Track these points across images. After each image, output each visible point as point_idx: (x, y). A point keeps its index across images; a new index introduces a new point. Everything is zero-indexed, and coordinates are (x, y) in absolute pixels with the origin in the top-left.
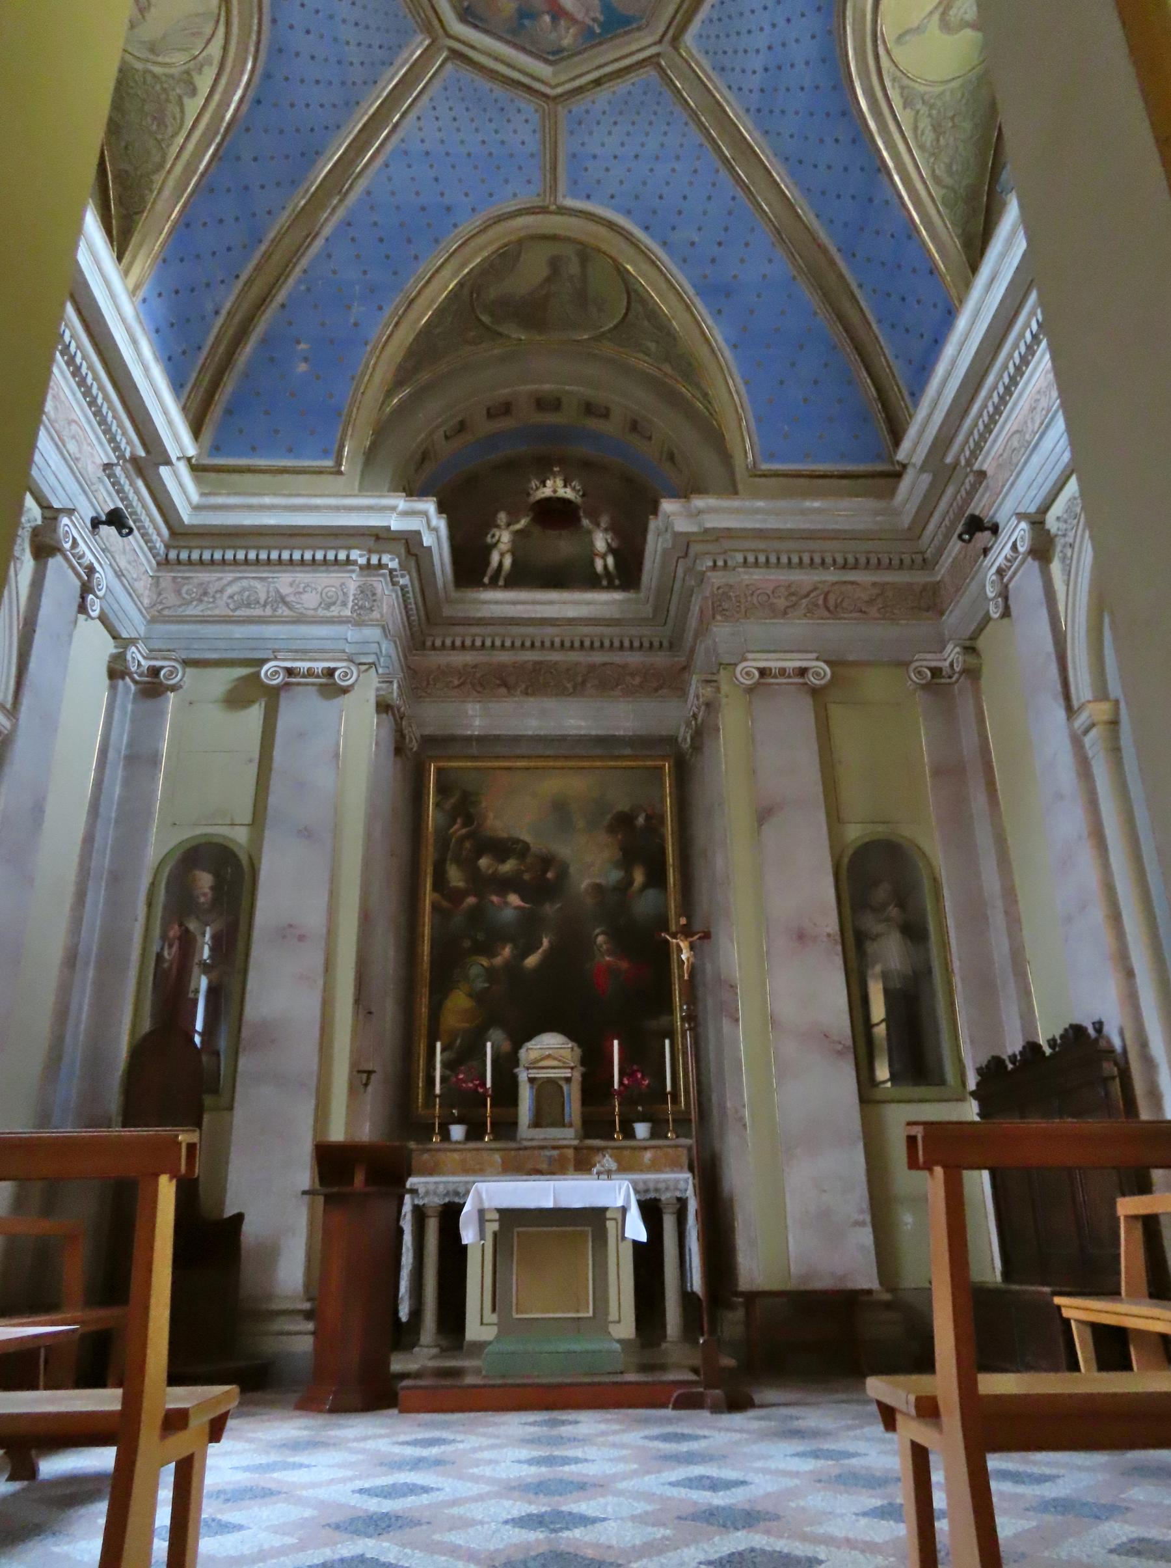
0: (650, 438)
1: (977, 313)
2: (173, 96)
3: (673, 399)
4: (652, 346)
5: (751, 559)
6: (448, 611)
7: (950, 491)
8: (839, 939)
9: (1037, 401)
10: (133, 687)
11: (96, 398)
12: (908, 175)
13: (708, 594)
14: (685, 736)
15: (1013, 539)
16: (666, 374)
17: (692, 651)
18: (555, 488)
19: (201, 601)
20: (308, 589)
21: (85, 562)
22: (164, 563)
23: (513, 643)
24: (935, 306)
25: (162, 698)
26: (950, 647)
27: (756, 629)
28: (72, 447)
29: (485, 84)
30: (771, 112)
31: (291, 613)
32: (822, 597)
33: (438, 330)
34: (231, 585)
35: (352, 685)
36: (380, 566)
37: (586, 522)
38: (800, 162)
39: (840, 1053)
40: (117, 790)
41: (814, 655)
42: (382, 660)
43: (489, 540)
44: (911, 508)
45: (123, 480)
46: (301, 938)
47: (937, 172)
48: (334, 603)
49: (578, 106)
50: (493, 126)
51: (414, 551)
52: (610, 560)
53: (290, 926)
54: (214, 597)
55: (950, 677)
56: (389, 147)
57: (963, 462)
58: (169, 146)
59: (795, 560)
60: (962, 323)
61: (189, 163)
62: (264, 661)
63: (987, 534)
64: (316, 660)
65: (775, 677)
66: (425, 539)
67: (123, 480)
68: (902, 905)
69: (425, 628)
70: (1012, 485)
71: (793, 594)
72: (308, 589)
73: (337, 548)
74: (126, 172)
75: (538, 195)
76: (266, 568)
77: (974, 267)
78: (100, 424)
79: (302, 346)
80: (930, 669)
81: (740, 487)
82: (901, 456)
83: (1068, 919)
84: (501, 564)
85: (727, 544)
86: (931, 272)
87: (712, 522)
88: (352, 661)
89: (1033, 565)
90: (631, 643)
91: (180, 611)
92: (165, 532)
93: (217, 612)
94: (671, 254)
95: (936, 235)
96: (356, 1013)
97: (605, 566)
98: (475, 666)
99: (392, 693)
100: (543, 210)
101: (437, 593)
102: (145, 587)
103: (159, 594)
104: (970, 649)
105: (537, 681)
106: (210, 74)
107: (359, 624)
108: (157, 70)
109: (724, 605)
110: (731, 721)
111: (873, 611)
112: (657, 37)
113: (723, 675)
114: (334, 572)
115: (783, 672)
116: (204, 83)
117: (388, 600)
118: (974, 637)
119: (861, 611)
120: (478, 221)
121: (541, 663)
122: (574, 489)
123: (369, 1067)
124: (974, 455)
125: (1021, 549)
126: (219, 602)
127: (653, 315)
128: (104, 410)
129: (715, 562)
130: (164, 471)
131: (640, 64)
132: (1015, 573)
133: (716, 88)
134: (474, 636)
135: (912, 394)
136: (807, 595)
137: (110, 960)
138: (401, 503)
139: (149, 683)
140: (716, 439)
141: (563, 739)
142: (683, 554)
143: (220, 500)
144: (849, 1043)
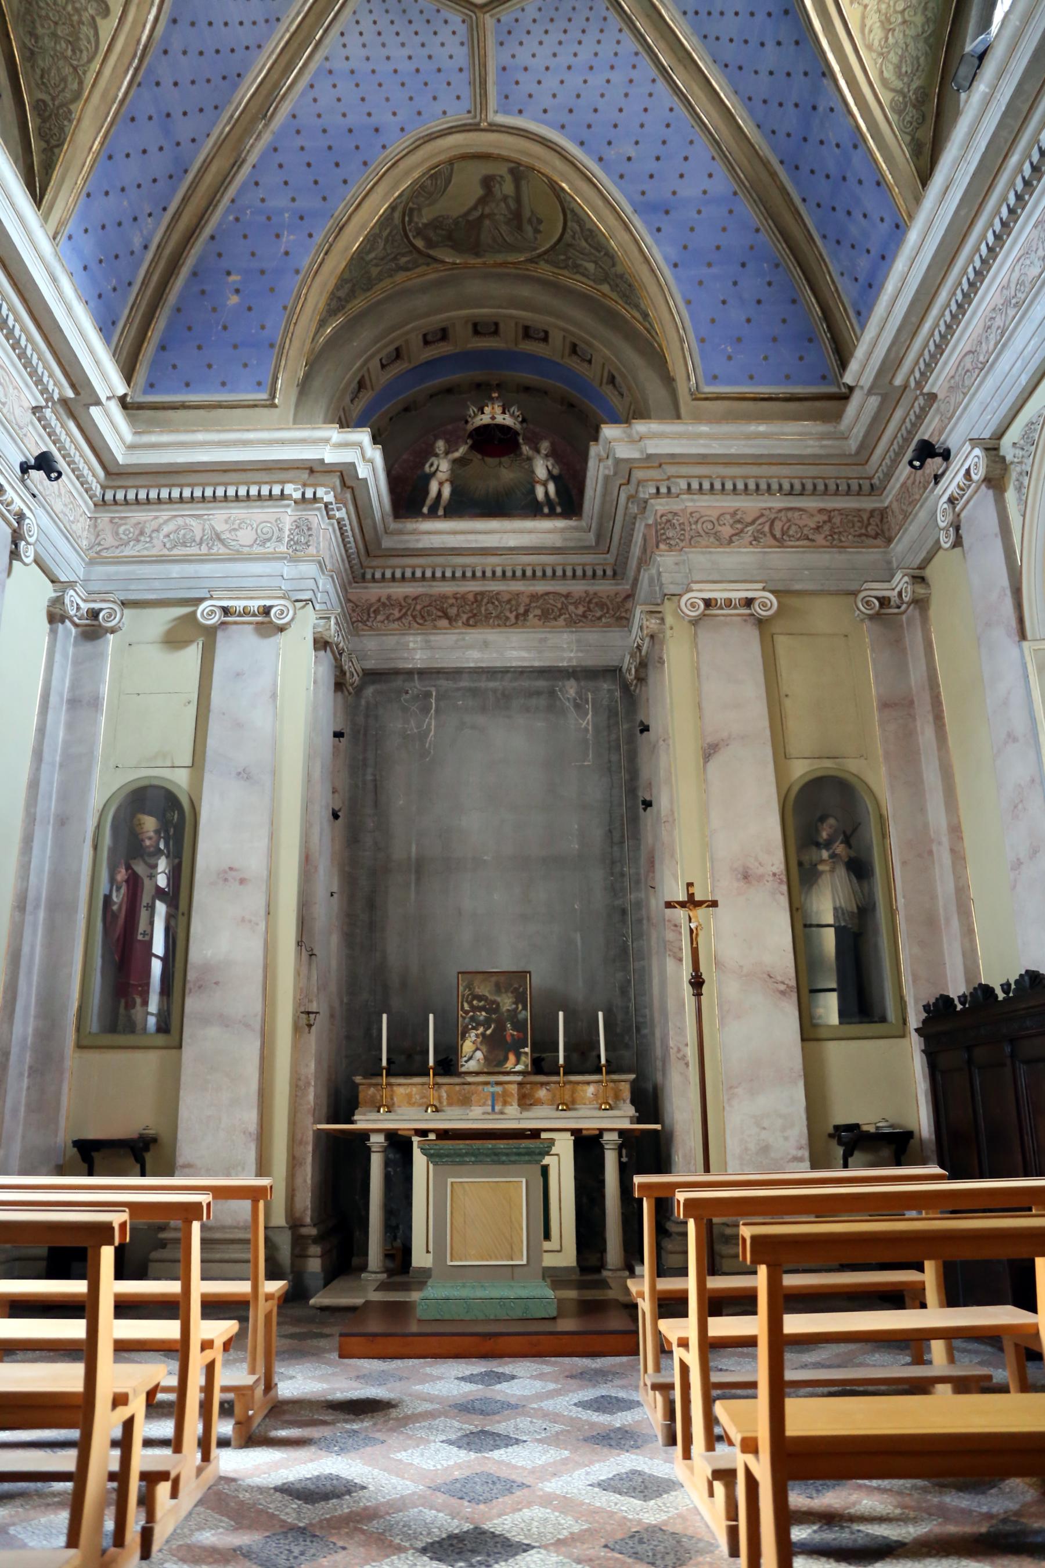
0: (590, 362)
2: (86, 16)
3: (611, 319)
4: (591, 267)
5: (695, 485)
6: (387, 543)
7: (899, 414)
8: (785, 879)
9: (993, 318)
10: (73, 630)
11: (18, 341)
12: (854, 77)
13: (650, 522)
14: (628, 664)
15: (966, 466)
16: (604, 295)
18: (494, 414)
19: (138, 541)
20: (243, 525)
21: (14, 508)
22: (102, 504)
23: (454, 573)
24: (882, 220)
25: (101, 641)
26: (898, 576)
27: (699, 558)
30: (709, 13)
31: (228, 551)
32: (768, 524)
33: (372, 255)
34: (166, 522)
35: (289, 624)
37: (525, 449)
38: (740, 68)
39: (783, 993)
40: (61, 734)
41: (760, 586)
42: (319, 595)
45: (54, 422)
46: (242, 881)
47: (885, 72)
48: (269, 540)
51: (349, 483)
52: (551, 488)
53: (231, 869)
54: (150, 536)
55: (899, 607)
56: (313, 66)
57: (912, 384)
58: (85, 73)
59: (740, 486)
60: (913, 236)
61: (106, 91)
62: (201, 600)
63: (939, 460)
64: (251, 598)
65: (721, 608)
67: (54, 422)
68: (847, 841)
69: (364, 560)
70: (965, 408)
71: (739, 522)
72: (243, 525)
74: (44, 101)
75: (469, 112)
76: (201, 505)
77: (925, 176)
79: (233, 278)
80: (877, 598)
81: (683, 411)
82: (848, 379)
83: (1017, 865)
84: (439, 494)
85: (671, 470)
86: (878, 184)
87: (654, 448)
88: (289, 599)
89: (987, 495)
90: (574, 571)
93: (154, 552)
94: (607, 170)
95: (886, 146)
96: (299, 953)
97: (547, 493)
98: (416, 598)
99: (329, 629)
100: (475, 128)
102: (83, 529)
103: (98, 535)
104: (919, 579)
105: (478, 612)
107: (293, 560)
109: (665, 533)
110: (676, 656)
111: (820, 539)
113: (668, 607)
114: (268, 507)
115: (729, 603)
117: (325, 540)
118: (922, 567)
119: (808, 539)
120: (407, 141)
121: (482, 594)
122: (512, 415)
123: (314, 1007)
125: (975, 477)
126: (155, 541)
127: (590, 234)
128: (29, 352)
129: (658, 489)
130: (94, 411)
132: (968, 502)
133: (287, 30)
134: (414, 567)
135: (859, 313)
136: (753, 522)
137: (58, 905)
138: (335, 434)
139: (87, 625)
140: (658, 360)
141: (505, 671)
142: (624, 481)
143: (153, 438)
144: (793, 983)
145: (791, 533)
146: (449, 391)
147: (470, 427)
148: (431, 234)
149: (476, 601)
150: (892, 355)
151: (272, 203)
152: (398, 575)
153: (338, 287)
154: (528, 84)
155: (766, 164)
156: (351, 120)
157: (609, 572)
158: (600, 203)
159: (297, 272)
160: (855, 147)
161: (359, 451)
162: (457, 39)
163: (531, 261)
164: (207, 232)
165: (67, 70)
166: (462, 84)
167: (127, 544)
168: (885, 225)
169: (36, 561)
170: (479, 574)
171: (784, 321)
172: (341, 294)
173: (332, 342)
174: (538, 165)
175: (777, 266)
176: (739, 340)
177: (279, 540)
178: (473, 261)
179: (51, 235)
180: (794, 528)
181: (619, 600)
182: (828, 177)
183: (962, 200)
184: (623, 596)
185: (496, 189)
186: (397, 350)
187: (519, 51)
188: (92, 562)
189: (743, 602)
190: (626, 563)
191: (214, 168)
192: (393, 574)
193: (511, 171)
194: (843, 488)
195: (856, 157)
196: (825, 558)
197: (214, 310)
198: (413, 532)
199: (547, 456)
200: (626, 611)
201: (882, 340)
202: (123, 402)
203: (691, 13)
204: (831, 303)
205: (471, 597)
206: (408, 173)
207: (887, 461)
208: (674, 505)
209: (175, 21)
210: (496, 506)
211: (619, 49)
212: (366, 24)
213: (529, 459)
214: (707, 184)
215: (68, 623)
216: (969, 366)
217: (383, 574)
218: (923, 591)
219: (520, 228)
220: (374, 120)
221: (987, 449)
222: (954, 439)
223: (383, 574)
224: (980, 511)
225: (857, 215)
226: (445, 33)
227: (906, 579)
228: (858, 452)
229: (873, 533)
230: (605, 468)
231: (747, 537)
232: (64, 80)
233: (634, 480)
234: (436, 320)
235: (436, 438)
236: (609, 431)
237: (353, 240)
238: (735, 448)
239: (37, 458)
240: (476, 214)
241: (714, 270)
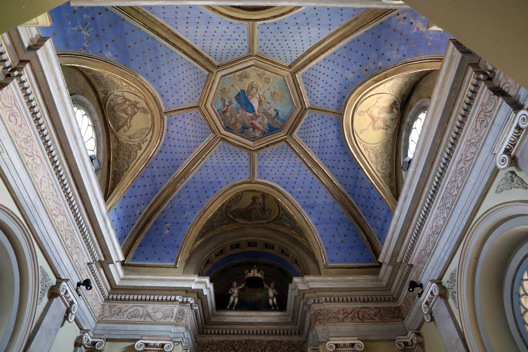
0: (288, 256)
1: (402, 209)
2: (134, 150)
4: (288, 225)
5: (328, 299)
6: (213, 319)
7: (400, 272)
15: (430, 290)
16: (293, 234)
17: (307, 337)
18: (254, 273)
19: (118, 314)
21: (70, 299)
22: (107, 300)
23: (238, 332)
27: (331, 327)
28: (75, 257)
29: (232, 147)
34: (130, 308)
36: (187, 302)
37: (265, 286)
41: (356, 338)
43: (230, 292)
44: (386, 278)
45: (95, 269)
48: (168, 317)
49: (261, 152)
50: (234, 158)
51: (200, 297)
52: (275, 300)
55: (412, 346)
56: (201, 165)
57: (404, 261)
60: (397, 213)
62: (138, 340)
63: (418, 288)
64: (157, 340)
65: (342, 348)
66: (204, 292)
67: (95, 269)
70: (426, 269)
73: (171, 295)
74: (116, 171)
77: (397, 197)
78: (88, 249)
82: (380, 260)
84: (234, 301)
85: (319, 294)
86: (381, 199)
87: (312, 285)
89: (441, 301)
91: (109, 319)
92: (109, 288)
93: (123, 319)
94: (293, 195)
95: (382, 188)
97: (273, 302)
98: (223, 342)
101: (209, 313)
102: (98, 309)
104: (418, 334)
106: (146, 144)
107: (176, 325)
108: (131, 143)
109: (317, 317)
111: (377, 319)
112: (285, 134)
113: (321, 347)
115: (345, 345)
116: (144, 147)
121: (248, 340)
122: (261, 274)
124: (408, 258)
126: (124, 315)
127: (288, 214)
129: (314, 301)
130: (111, 266)
131: (281, 141)
134: (223, 329)
136: (351, 313)
138: (196, 278)
139: (90, 348)
140: (312, 255)
145: (366, 317)
146: (239, 265)
147: (246, 277)
148: (235, 214)
149: (246, 343)
150: (395, 252)
151: (183, 203)
152: (216, 332)
153: (202, 229)
154: (267, 171)
155: (344, 194)
156: (211, 180)
157: (297, 332)
158: (291, 205)
159: (189, 224)
160: (372, 188)
161: (205, 285)
162: (246, 159)
163: (268, 223)
164: (161, 210)
165: (125, 163)
166: (247, 171)
167: (113, 316)
168: (385, 211)
169: (75, 320)
170: (247, 332)
171: (354, 242)
172: (203, 231)
173: (199, 247)
174: (270, 193)
175: (350, 224)
176: (340, 248)
177: (172, 317)
178: (249, 222)
179: (108, 209)
180: (366, 315)
181: (301, 343)
182: (364, 197)
183: (412, 201)
184: (303, 341)
185: (257, 200)
186: (222, 250)
187: (265, 162)
188: (98, 322)
189: (350, 345)
190: (303, 329)
191: (167, 191)
192: (215, 332)
193: (262, 195)
194: (383, 299)
195: (373, 191)
196: (380, 327)
197: (160, 235)
198: (223, 316)
199: (273, 288)
200: (304, 348)
201: (391, 247)
202: (123, 264)
203: (317, 153)
204: (370, 236)
205: (244, 342)
206: (228, 195)
207: (398, 289)
208: (321, 307)
209: (161, 152)
210: (255, 306)
211: (295, 162)
212: (218, 154)
213: (267, 289)
214: (325, 200)
215: (82, 347)
216: (423, 254)
217: (211, 332)
218: (421, 339)
219: (264, 212)
220: (218, 180)
221: (437, 284)
222: (424, 279)
223: (211, 332)
224: (440, 307)
225: (375, 208)
226: (242, 157)
227: (413, 334)
228: (387, 286)
229: (396, 316)
230: (295, 293)
231: (349, 319)
232: (124, 165)
233: (305, 298)
234: (236, 241)
235: (234, 281)
236: (296, 280)
237: (209, 215)
238: (342, 285)
239: (84, 281)
240: (250, 208)
241: (330, 225)
